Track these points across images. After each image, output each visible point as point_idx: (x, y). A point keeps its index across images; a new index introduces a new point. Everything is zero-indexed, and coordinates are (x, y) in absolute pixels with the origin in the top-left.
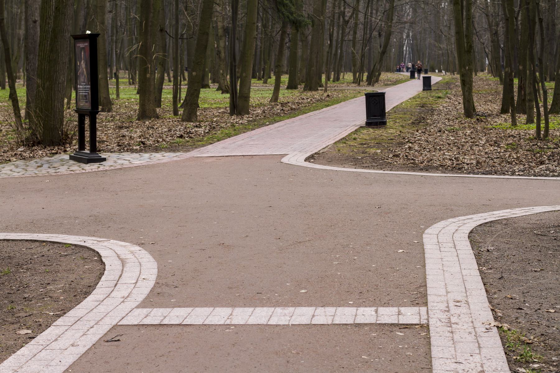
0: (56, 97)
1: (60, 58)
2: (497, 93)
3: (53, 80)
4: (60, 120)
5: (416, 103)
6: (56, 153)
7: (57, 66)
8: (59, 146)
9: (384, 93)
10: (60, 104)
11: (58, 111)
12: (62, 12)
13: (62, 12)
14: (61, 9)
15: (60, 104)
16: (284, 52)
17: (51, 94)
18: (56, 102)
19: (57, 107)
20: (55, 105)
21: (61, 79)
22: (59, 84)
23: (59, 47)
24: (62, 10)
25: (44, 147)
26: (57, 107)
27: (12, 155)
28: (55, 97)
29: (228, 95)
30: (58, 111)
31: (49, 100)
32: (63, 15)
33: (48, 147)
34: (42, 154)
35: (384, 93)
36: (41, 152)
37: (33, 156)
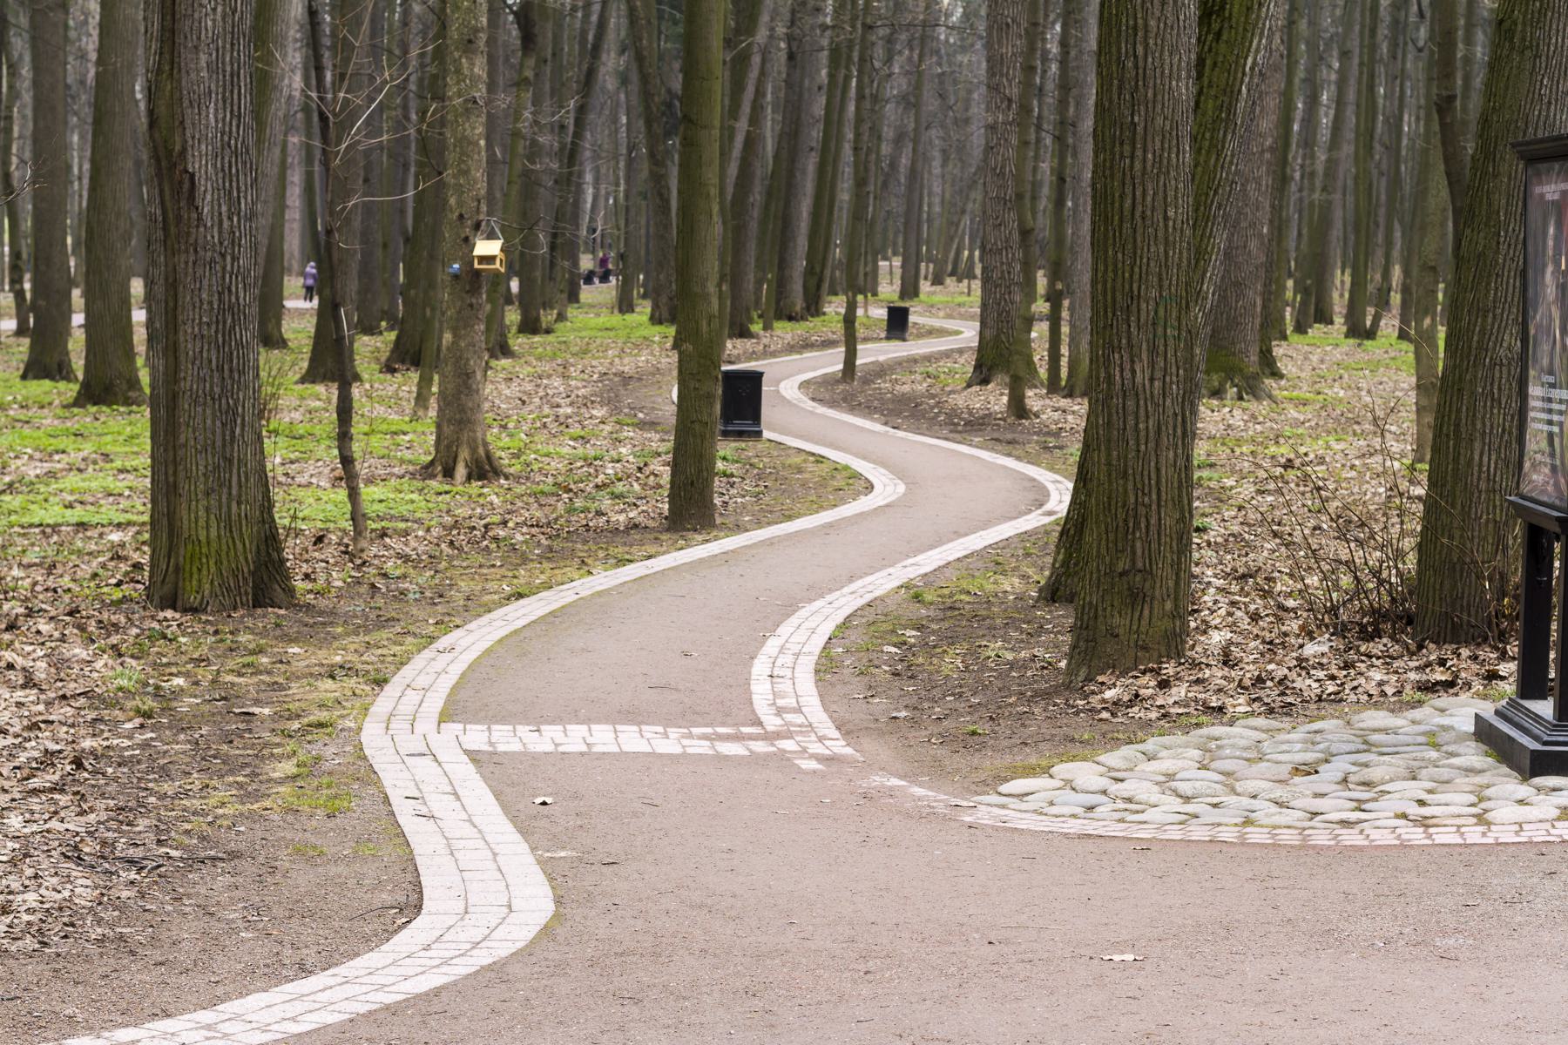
0: (1479, 426)
1: (1504, 247)
2: (18, 369)
3: (1470, 347)
4: (1491, 526)
5: (255, 679)
6: (1449, 685)
7: (1488, 284)
8: (1479, 645)
9: (761, 374)
10: (1493, 457)
11: (1483, 485)
12: (1523, 39)
13: (1523, 39)
14: (1520, 27)
15: (1493, 457)
16: (1487, 50)
17: (1459, 411)
18: (1477, 445)
19: (1480, 471)
20: (1472, 459)
21: (1505, 344)
22: (1493, 365)
23: (1503, 202)
24: (1524, 31)
25: (1413, 647)
26: (1480, 471)
27: (1240, 685)
28: (1474, 424)
29: (1080, 407)
30: (1483, 485)
31: (1448, 435)
32: (1528, 53)
33: (1432, 646)
34: (1380, 684)
35: (761, 374)
36: (1377, 676)
37: (1336, 693)
